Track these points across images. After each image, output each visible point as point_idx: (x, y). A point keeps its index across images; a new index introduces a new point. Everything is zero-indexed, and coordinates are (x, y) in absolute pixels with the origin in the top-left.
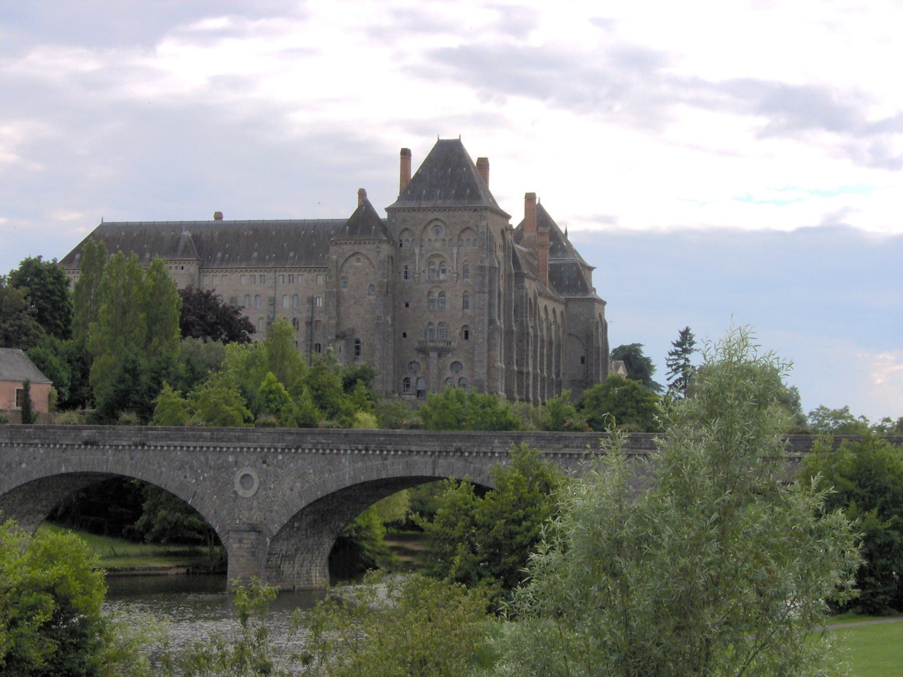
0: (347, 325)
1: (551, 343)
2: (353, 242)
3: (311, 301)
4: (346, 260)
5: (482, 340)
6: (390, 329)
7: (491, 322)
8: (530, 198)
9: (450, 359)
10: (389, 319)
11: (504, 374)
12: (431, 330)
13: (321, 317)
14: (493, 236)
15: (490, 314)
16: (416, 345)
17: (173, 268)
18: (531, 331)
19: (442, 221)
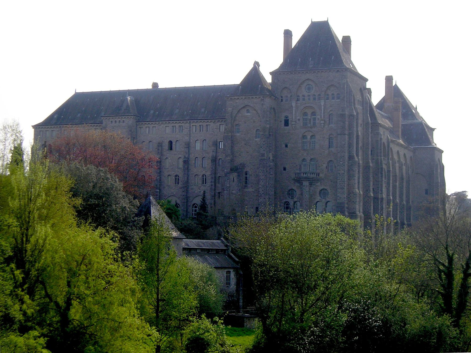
0: (239, 161)
1: (402, 178)
2: (244, 97)
3: (216, 144)
4: (239, 111)
5: (343, 172)
6: (271, 164)
7: (351, 157)
8: (389, 79)
9: (319, 187)
10: (271, 155)
11: (362, 198)
12: (305, 165)
13: (221, 156)
14: (352, 91)
15: (349, 152)
16: (293, 176)
17: (114, 122)
18: (384, 166)
19: (312, 81)
